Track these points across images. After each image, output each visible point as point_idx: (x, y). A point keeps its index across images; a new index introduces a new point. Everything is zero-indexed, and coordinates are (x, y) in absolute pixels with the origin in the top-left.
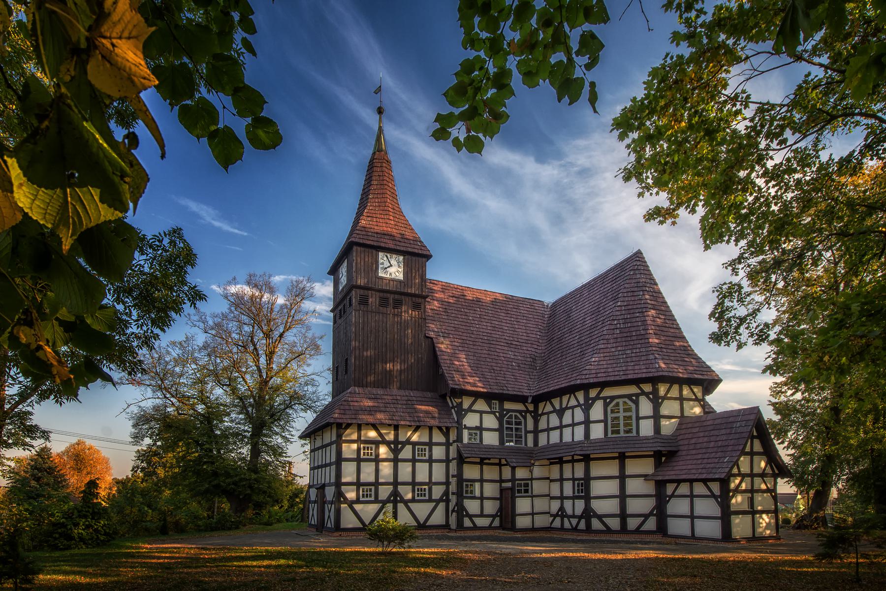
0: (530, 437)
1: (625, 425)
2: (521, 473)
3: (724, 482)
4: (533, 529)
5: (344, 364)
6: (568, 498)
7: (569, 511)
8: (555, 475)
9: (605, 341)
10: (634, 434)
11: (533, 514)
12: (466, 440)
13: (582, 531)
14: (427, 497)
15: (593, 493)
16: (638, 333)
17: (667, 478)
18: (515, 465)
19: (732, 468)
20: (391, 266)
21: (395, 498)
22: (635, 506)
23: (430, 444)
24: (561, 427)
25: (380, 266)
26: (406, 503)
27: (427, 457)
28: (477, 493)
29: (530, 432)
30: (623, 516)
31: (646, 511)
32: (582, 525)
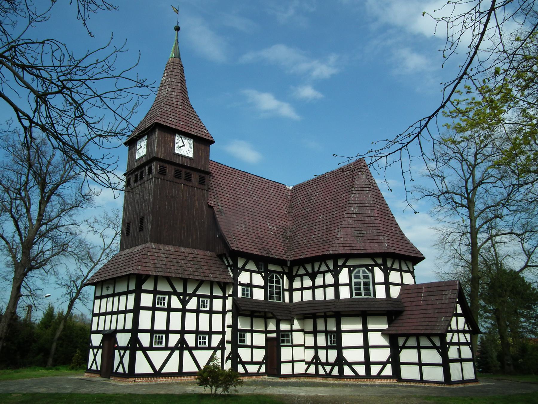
0: (287, 294)
1: (365, 289)
2: (284, 327)
3: (443, 337)
4: (293, 375)
5: (138, 221)
6: (322, 348)
7: (323, 359)
8: (310, 328)
9: (346, 222)
10: (372, 296)
11: (293, 362)
12: (240, 295)
13: (335, 377)
14: (207, 345)
15: (344, 344)
16: (369, 218)
17: (400, 332)
18: (280, 318)
19: (448, 328)
20: (184, 145)
21: (182, 346)
22: (376, 355)
23: (211, 297)
24: (314, 288)
25: (176, 145)
26: (190, 349)
27: (166, 306)
28: (248, 343)
29: (286, 290)
30: (367, 363)
31: (384, 359)
32: (336, 372)
